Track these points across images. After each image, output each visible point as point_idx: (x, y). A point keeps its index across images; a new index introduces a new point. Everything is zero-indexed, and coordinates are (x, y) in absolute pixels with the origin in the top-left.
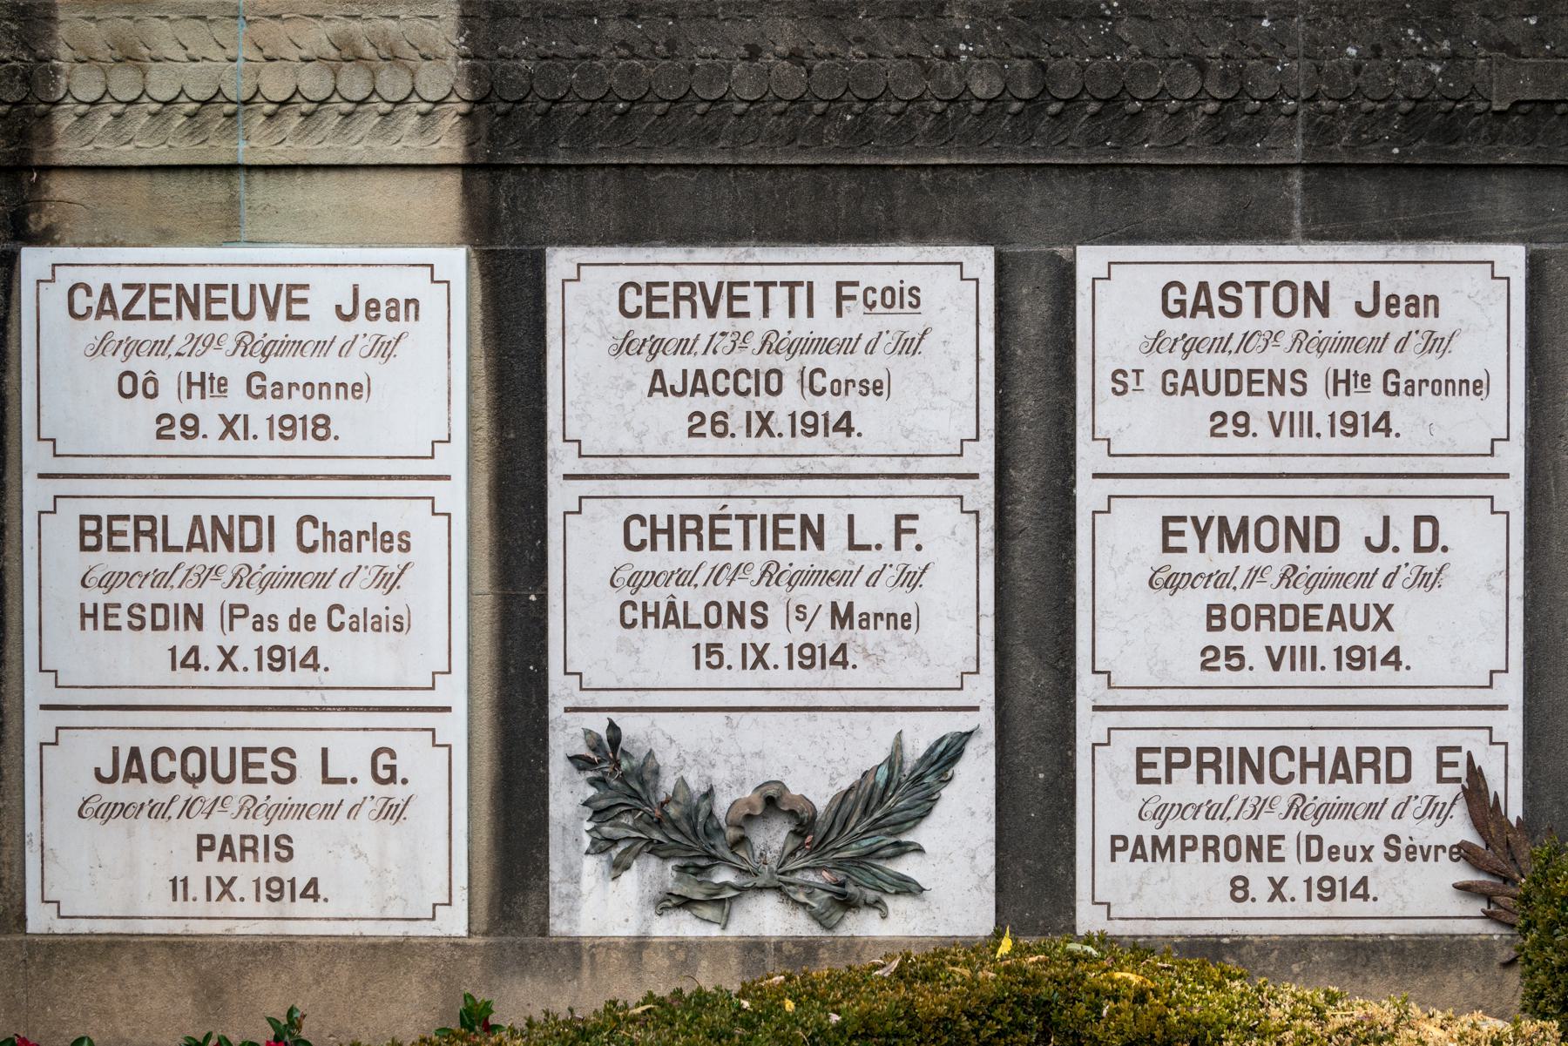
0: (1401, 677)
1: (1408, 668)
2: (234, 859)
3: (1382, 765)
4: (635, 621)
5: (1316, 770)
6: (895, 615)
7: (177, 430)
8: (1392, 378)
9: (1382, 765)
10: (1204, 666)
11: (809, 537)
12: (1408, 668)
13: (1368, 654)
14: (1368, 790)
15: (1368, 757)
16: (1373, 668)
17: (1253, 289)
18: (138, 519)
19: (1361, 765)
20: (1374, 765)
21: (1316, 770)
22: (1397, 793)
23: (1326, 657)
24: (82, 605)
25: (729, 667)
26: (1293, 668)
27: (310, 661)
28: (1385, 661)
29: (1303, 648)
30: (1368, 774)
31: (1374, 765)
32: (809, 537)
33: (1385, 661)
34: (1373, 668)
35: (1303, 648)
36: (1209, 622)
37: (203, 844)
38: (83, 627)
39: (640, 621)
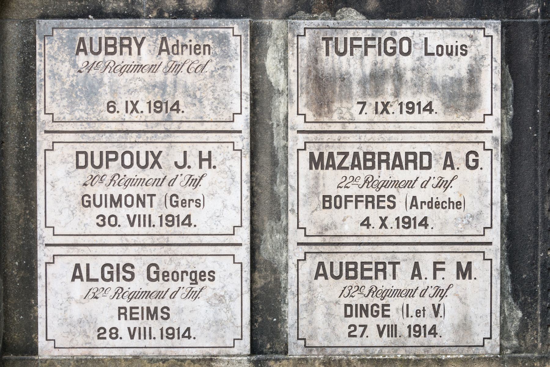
0: (429, 231)
1: (195, 226)
2: (417, 208)
3: (418, 161)
4: (446, 207)
5: (207, 162)
6: (336, 207)
7: (107, 335)
8: (174, 198)
9: (418, 161)
10: (350, 336)
11: (142, 199)
12: (195, 226)
13: (176, 219)
14: (410, 174)
15: (411, 157)
16: (415, 227)
17: (149, 197)
18: (377, 263)
19: (407, 161)
20: (414, 161)
21: (207, 162)
22: (424, 175)
23: (123, 220)
24: (200, 153)
25: (412, 316)
26: (139, 225)
27: (187, 222)
28: (420, 224)
29: (144, 216)
30: (411, 165)
31: (414, 161)
32: (142, 199)
33: (420, 224)
34: (415, 227)
35: (144, 216)
36: (324, 204)
37: (122, 312)
38: (119, 319)
39: (448, 207)
